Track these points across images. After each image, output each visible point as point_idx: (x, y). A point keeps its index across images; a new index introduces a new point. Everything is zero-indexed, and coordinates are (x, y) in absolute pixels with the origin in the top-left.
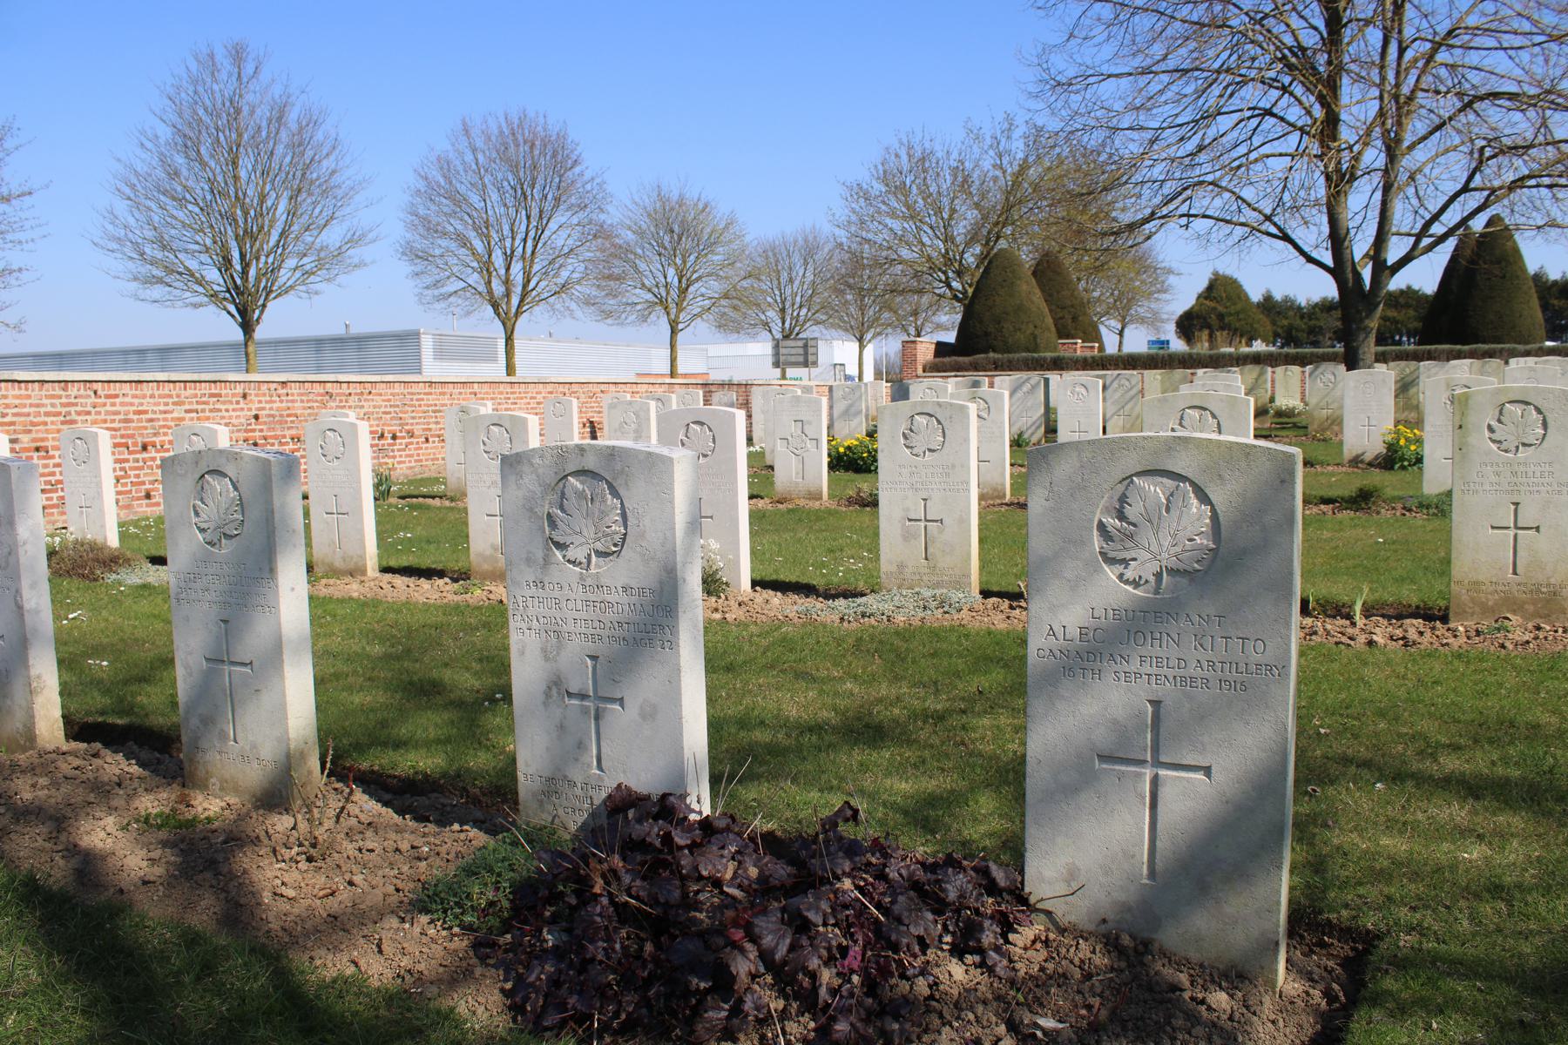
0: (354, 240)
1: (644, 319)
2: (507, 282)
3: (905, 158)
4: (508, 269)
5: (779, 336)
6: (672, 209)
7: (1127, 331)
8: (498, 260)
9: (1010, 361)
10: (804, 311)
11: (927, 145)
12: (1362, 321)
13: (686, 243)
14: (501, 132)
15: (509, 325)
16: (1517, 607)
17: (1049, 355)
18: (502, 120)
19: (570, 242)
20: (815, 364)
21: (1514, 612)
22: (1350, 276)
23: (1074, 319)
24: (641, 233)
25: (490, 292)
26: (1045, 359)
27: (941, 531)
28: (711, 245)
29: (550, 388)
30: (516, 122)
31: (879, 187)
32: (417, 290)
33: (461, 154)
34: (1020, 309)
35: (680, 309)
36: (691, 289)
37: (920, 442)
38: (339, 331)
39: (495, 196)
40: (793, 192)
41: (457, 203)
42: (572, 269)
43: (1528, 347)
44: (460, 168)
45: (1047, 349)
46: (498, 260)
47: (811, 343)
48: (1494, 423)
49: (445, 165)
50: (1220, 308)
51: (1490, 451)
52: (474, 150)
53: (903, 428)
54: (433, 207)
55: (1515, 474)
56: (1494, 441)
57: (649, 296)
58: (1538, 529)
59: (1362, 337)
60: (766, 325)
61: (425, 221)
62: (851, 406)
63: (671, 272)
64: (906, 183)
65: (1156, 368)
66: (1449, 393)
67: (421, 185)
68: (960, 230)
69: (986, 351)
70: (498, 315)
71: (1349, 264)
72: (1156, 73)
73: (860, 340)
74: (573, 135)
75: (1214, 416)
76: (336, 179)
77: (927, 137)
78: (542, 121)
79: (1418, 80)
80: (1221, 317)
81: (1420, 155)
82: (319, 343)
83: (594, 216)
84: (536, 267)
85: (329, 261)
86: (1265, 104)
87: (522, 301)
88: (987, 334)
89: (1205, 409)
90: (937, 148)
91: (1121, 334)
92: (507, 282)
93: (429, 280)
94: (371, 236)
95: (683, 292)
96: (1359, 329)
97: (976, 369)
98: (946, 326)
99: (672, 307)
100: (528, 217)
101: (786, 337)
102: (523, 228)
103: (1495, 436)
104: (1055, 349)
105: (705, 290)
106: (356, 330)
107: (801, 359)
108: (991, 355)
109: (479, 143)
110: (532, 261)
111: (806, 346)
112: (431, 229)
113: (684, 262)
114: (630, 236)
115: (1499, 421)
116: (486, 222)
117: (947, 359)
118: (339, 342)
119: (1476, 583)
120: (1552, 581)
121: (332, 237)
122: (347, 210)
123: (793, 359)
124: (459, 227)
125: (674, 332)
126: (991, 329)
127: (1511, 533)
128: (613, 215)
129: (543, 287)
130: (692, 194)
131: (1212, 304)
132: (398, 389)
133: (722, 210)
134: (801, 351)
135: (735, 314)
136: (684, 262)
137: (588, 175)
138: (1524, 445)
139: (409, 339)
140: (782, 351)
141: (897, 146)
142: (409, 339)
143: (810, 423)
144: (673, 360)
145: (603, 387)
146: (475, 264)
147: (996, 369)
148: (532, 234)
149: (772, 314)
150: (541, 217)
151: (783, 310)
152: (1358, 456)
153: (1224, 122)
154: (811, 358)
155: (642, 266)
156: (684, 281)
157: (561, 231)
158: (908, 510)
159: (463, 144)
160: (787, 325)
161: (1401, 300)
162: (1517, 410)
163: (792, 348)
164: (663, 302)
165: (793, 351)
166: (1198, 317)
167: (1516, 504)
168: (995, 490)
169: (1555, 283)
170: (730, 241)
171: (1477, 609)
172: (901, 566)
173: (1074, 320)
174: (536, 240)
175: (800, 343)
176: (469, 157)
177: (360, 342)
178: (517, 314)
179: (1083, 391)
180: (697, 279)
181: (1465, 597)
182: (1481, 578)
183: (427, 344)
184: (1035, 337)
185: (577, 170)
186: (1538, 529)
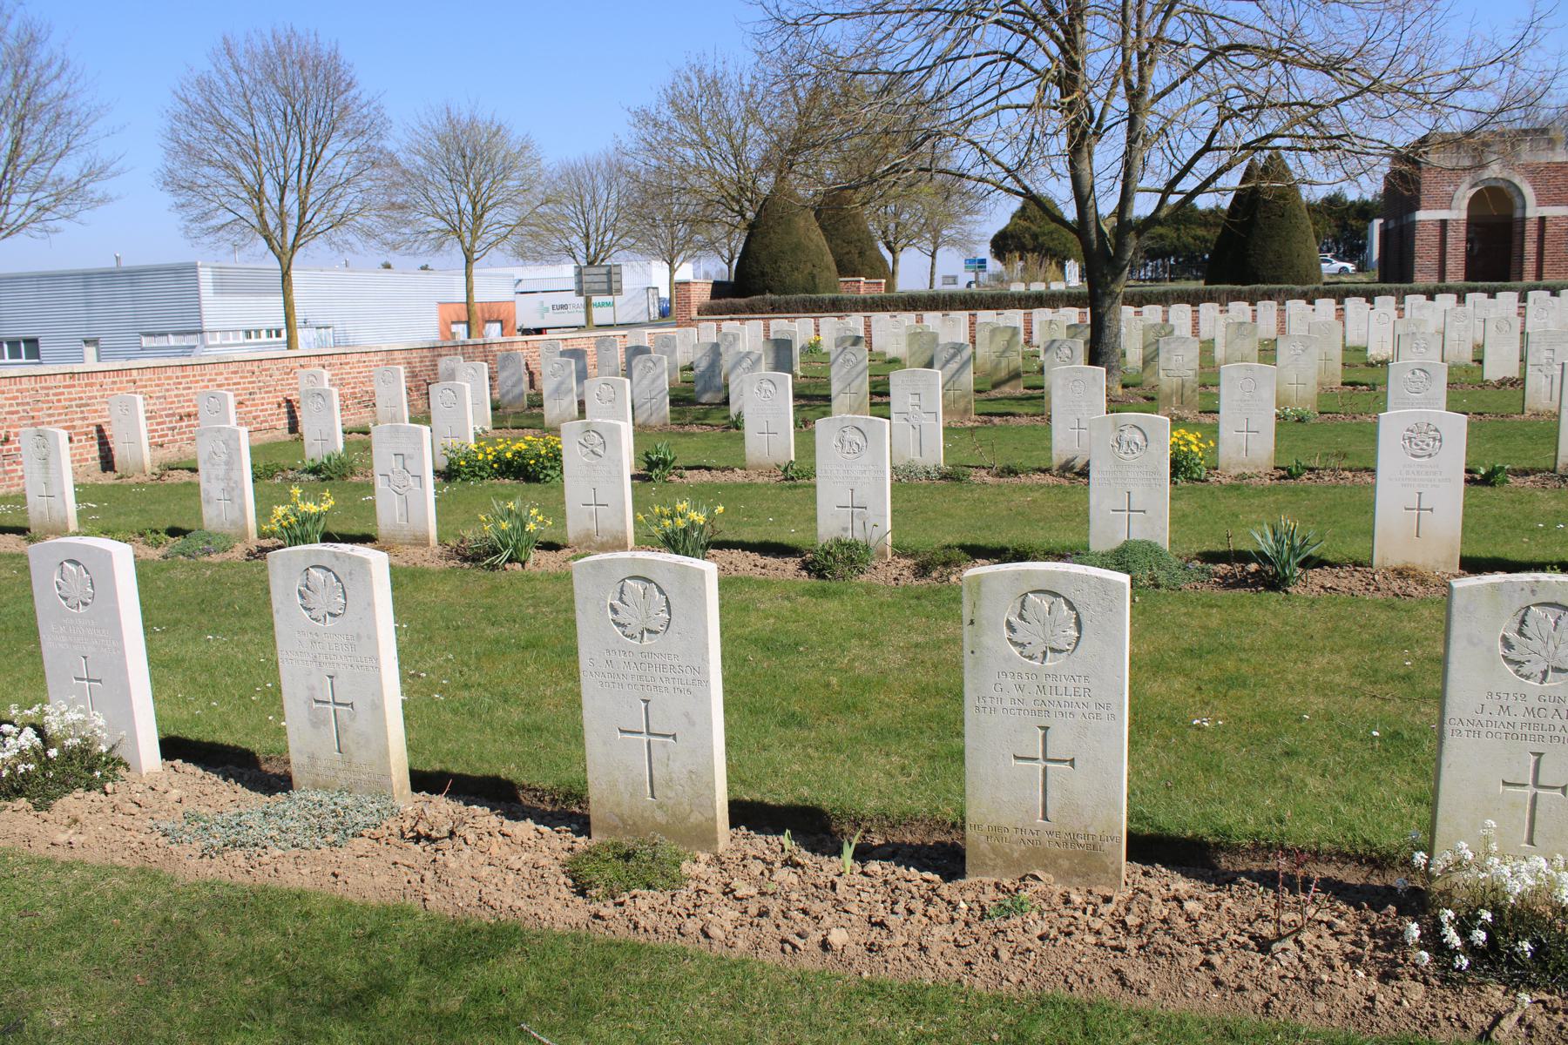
0: (94, 173)
1: (439, 247)
2: (282, 215)
3: (695, 81)
4: (281, 200)
5: (583, 263)
6: (463, 132)
7: (939, 252)
8: (270, 189)
9: (787, 303)
10: (609, 235)
11: (719, 67)
12: (1107, 285)
13: (479, 168)
14: (267, 52)
15: (285, 260)
16: (1049, 863)
17: (827, 295)
18: (269, 38)
19: (348, 170)
20: (619, 291)
21: (1045, 868)
22: (1094, 236)
23: (861, 254)
24: (429, 158)
25: (265, 225)
26: (823, 300)
27: (353, 719)
28: (506, 170)
29: (233, 368)
30: (284, 41)
31: (666, 113)
32: (182, 224)
33: (224, 76)
34: (797, 247)
35: (474, 237)
36: (486, 216)
37: (321, 602)
38: (109, 264)
39: (262, 122)
40: (582, 118)
41: (223, 129)
42: (349, 200)
43: (1305, 288)
44: (224, 89)
45: (827, 289)
46: (270, 189)
47: (614, 270)
48: (1014, 619)
49: (205, 85)
50: (1034, 228)
51: (1011, 657)
52: (238, 70)
53: (298, 584)
54: (196, 134)
55: (1041, 689)
56: (1015, 644)
57: (442, 225)
58: (1072, 762)
59: (1108, 301)
60: (570, 252)
61: (189, 148)
62: (561, 383)
63: (464, 199)
64: (698, 104)
65: (936, 309)
66: (1117, 433)
67: (181, 108)
68: (754, 154)
69: (763, 293)
70: (273, 249)
71: (1093, 225)
72: (889, 13)
73: (671, 264)
74: (346, 55)
75: (661, 592)
76: (68, 105)
77: (720, 59)
78: (313, 38)
79: (1160, 28)
80: (1035, 237)
81: (1171, 103)
82: (87, 278)
83: (372, 143)
84: (311, 199)
85: (69, 195)
86: (1011, 49)
87: (300, 229)
88: (763, 274)
89: (650, 581)
90: (731, 70)
91: (933, 256)
92: (282, 215)
93: (196, 212)
94: (113, 169)
95: (478, 218)
96: (1104, 294)
97: (753, 312)
98: (718, 268)
99: (467, 235)
100: (303, 144)
101: (590, 264)
102: (298, 156)
103: (1017, 637)
104: (835, 289)
105: (500, 217)
106: (126, 263)
107: (605, 287)
108: (768, 296)
109: (244, 64)
110: (307, 190)
111: (609, 273)
112: (192, 154)
113: (478, 188)
114: (420, 161)
115: (1021, 617)
116: (256, 150)
117: (723, 301)
118: (109, 276)
119: (997, 828)
120: (1091, 831)
121: (69, 168)
122: (86, 138)
123: (596, 287)
124: (225, 154)
125: (469, 261)
126: (768, 269)
127: (1040, 766)
128: (395, 142)
129: (318, 220)
130: (484, 116)
131: (1026, 224)
132: (26, 384)
133: (516, 134)
134: (605, 278)
135: (534, 241)
136: (478, 188)
137: (364, 98)
138: (1053, 650)
139: (185, 273)
140: (585, 278)
141: (686, 69)
142: (185, 273)
143: (411, 457)
144: (469, 291)
145: (302, 361)
146: (244, 195)
147: (773, 311)
148: (307, 159)
149: (575, 239)
150: (314, 146)
151: (587, 236)
152: (1068, 462)
153: (960, 70)
154: (615, 286)
155: (433, 194)
156: (479, 207)
157: (337, 158)
158: (312, 688)
159: (226, 65)
160: (592, 250)
161: (1210, 218)
162: (1044, 602)
163: (595, 276)
164: (455, 230)
165: (596, 279)
166: (1012, 237)
167: (1046, 729)
168: (615, 538)
169: (1353, 203)
170: (525, 166)
171: (1000, 862)
172: (312, 757)
173: (856, 257)
174: (312, 168)
175: (604, 271)
176: (233, 79)
177: (133, 276)
178: (294, 247)
179: (771, 387)
180: (494, 205)
181: (984, 846)
182: (1004, 822)
183: (206, 277)
184: (813, 277)
185: (353, 92)
186: (1072, 762)
